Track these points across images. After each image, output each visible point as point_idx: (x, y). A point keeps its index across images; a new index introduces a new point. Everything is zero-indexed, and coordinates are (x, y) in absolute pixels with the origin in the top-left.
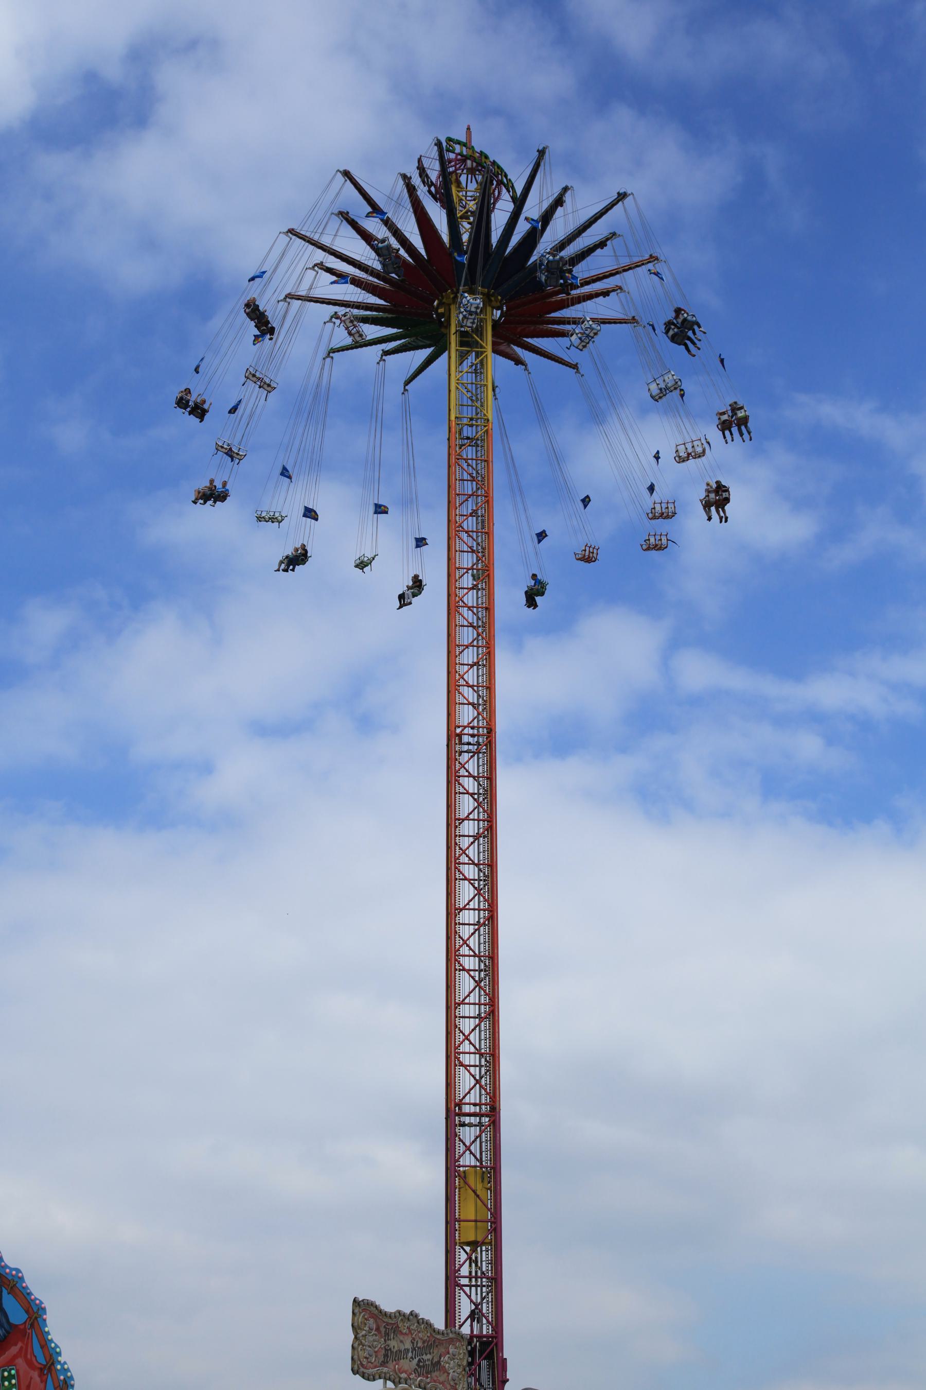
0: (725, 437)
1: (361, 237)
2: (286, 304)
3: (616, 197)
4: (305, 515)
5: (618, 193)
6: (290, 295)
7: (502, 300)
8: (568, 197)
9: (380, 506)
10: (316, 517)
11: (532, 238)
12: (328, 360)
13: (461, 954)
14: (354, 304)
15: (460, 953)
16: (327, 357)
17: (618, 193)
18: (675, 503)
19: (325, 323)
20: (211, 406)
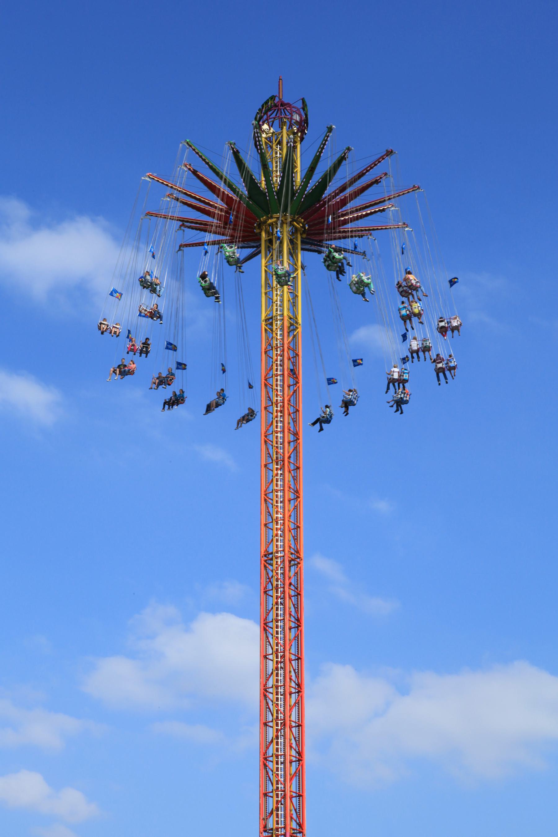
0: (439, 379)
1: (197, 177)
2: (182, 231)
3: (385, 153)
4: (167, 348)
5: (387, 150)
6: (150, 213)
7: (304, 222)
8: (349, 155)
9: (171, 344)
10: (176, 349)
11: (344, 202)
12: (180, 252)
13: (268, 687)
14: (210, 224)
15: (267, 687)
16: (178, 251)
17: (387, 150)
18: (389, 401)
19: (366, 300)
20: (452, 336)
